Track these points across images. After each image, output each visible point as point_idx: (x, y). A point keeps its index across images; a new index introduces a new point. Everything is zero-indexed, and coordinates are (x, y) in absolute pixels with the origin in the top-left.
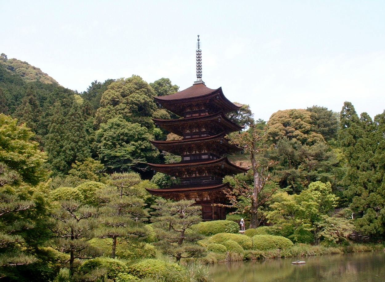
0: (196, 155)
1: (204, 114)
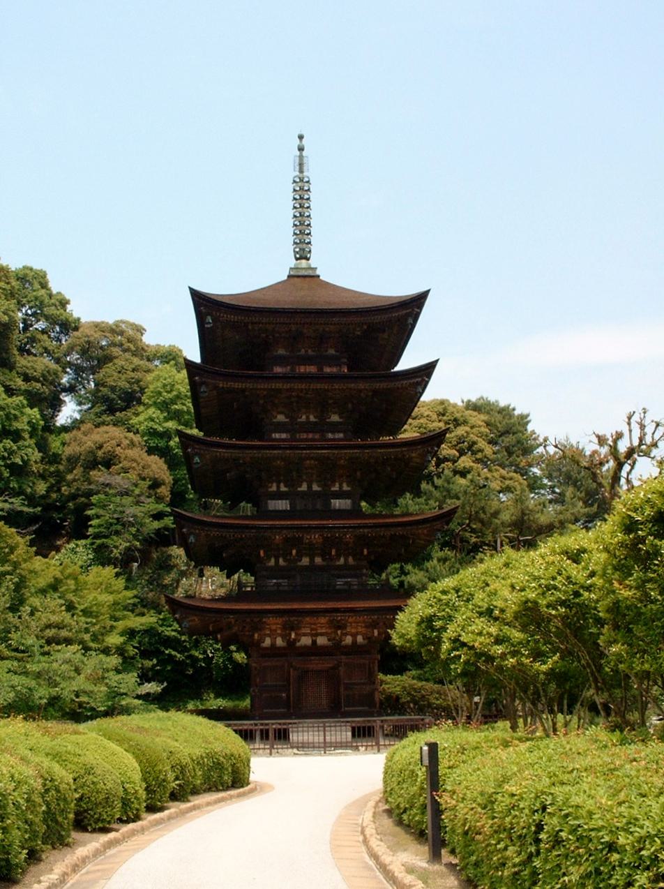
0: (309, 494)
1: (335, 370)
